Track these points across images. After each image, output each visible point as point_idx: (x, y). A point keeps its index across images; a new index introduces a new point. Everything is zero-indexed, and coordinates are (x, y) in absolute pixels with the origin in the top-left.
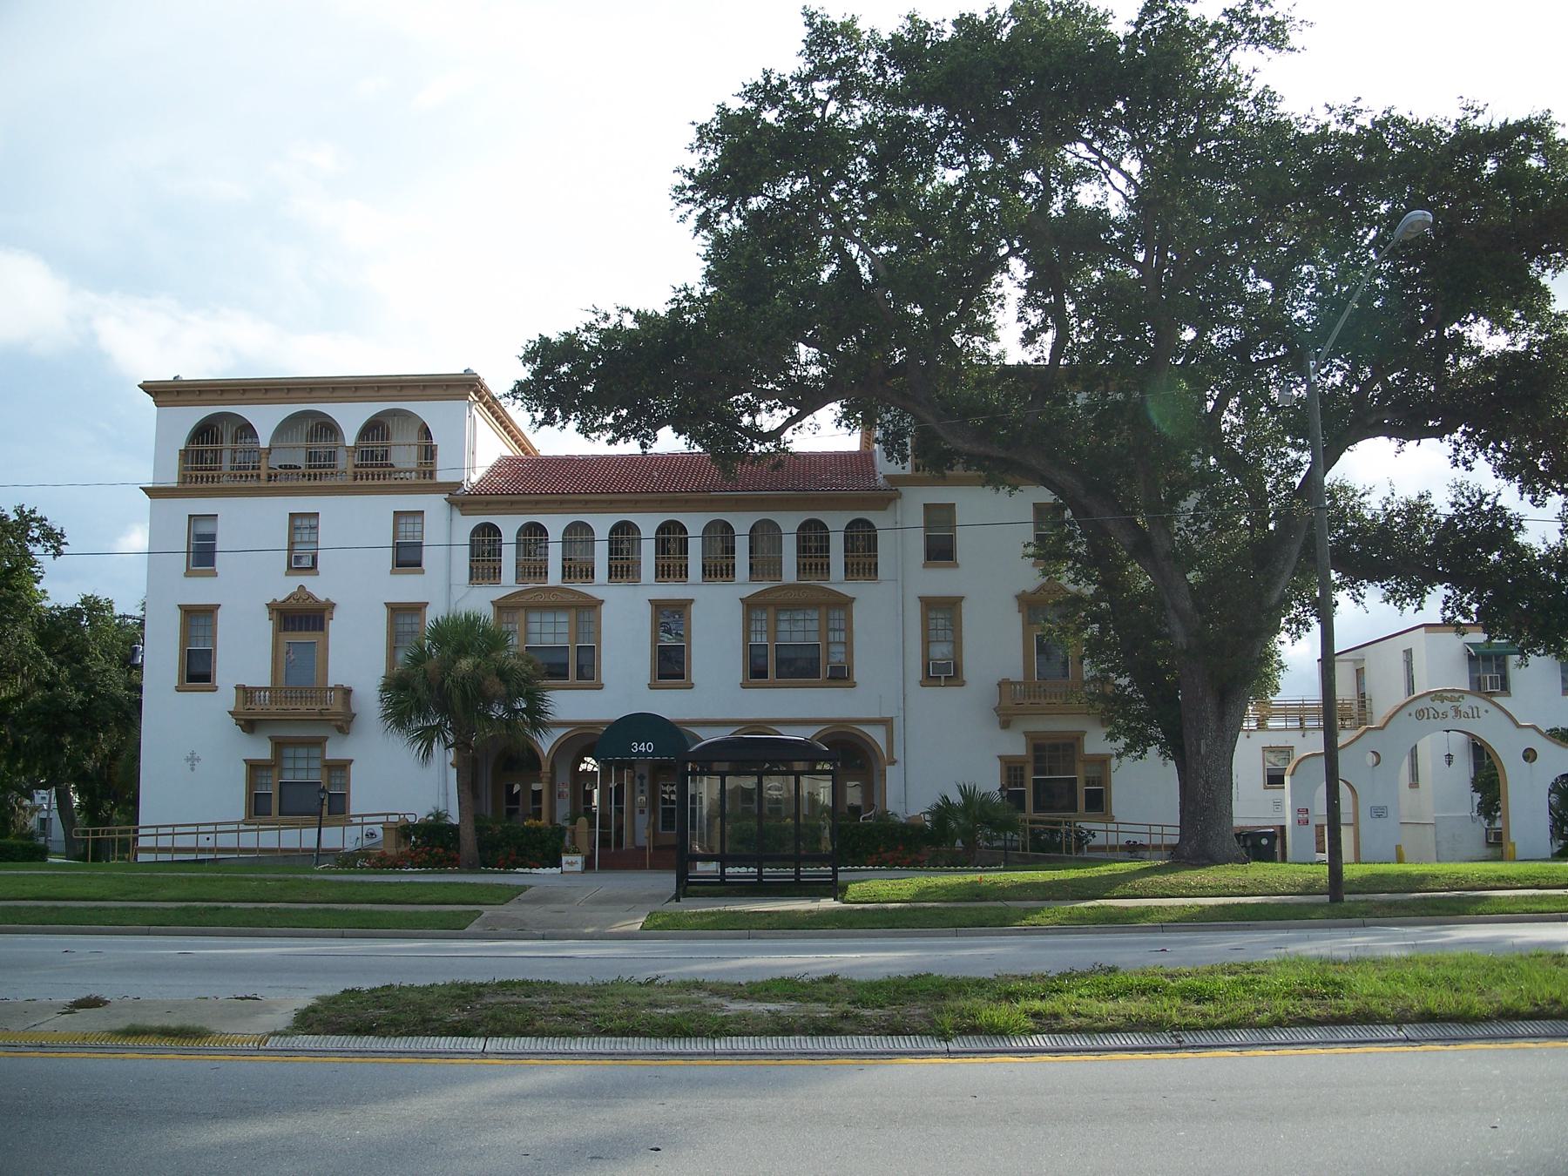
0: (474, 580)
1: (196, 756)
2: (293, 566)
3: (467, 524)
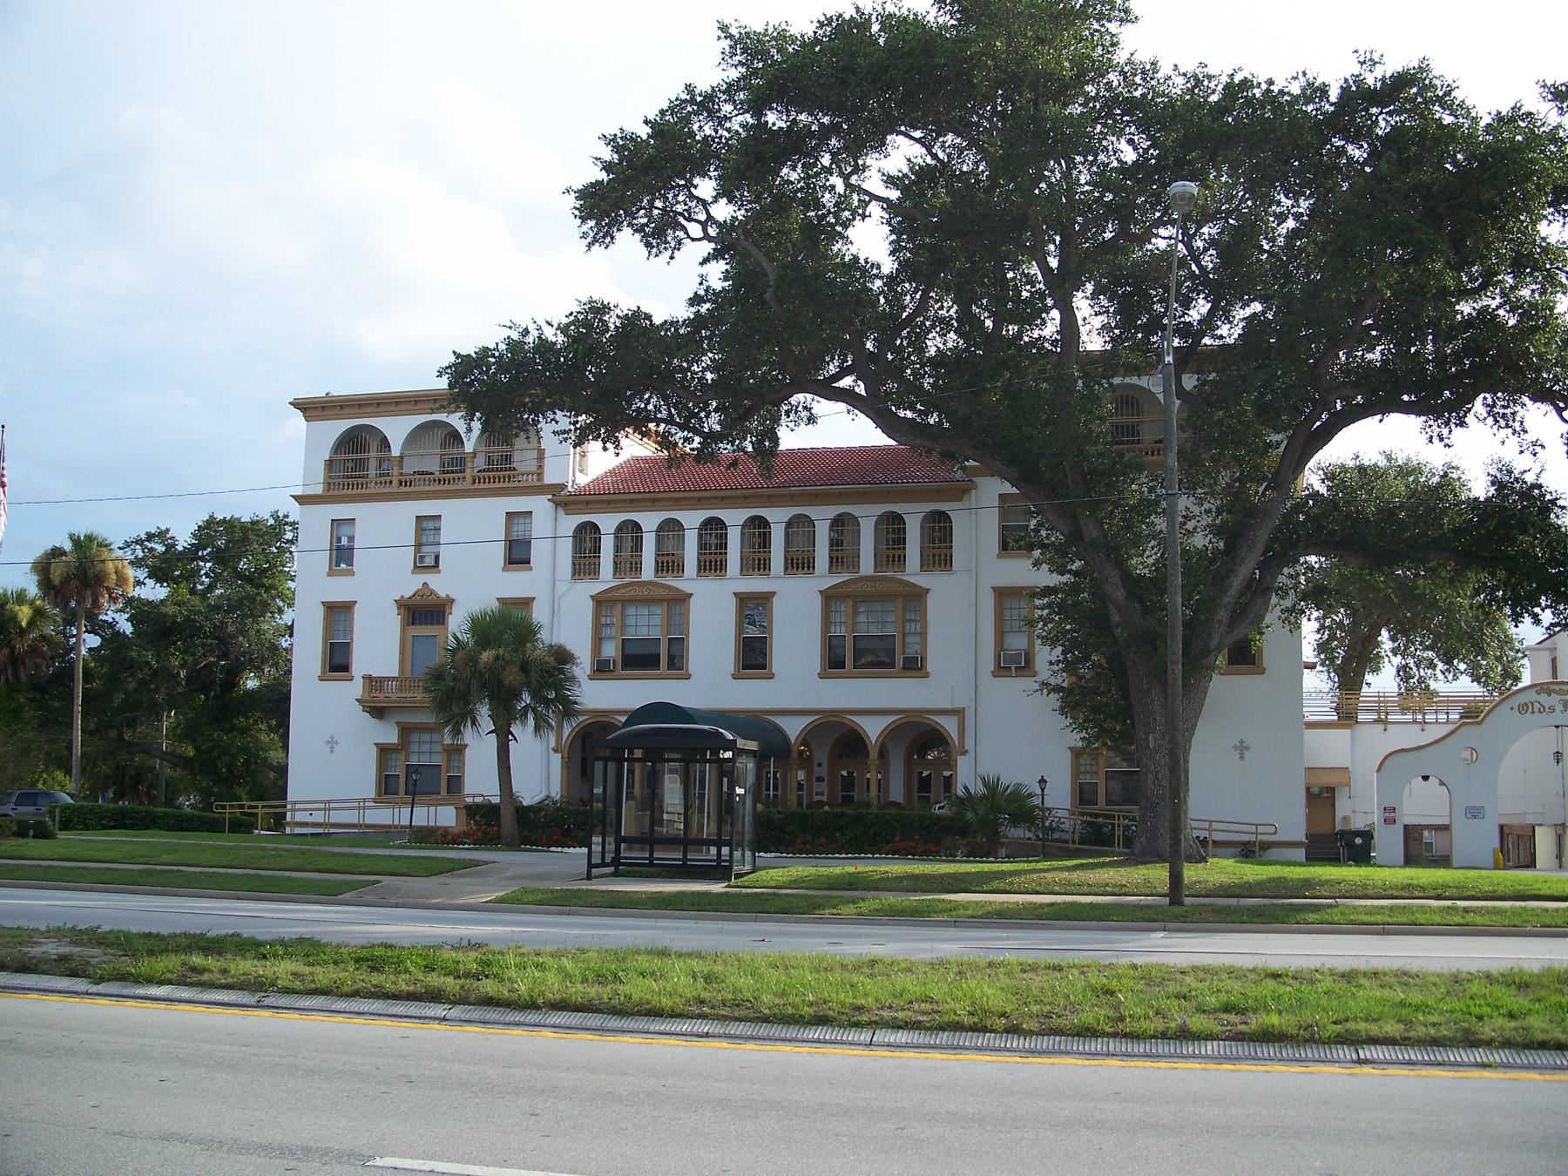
0: (789, 571)
3: (570, 523)
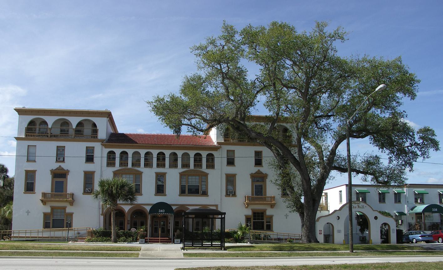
1: (29, 211)
2: (58, 160)
